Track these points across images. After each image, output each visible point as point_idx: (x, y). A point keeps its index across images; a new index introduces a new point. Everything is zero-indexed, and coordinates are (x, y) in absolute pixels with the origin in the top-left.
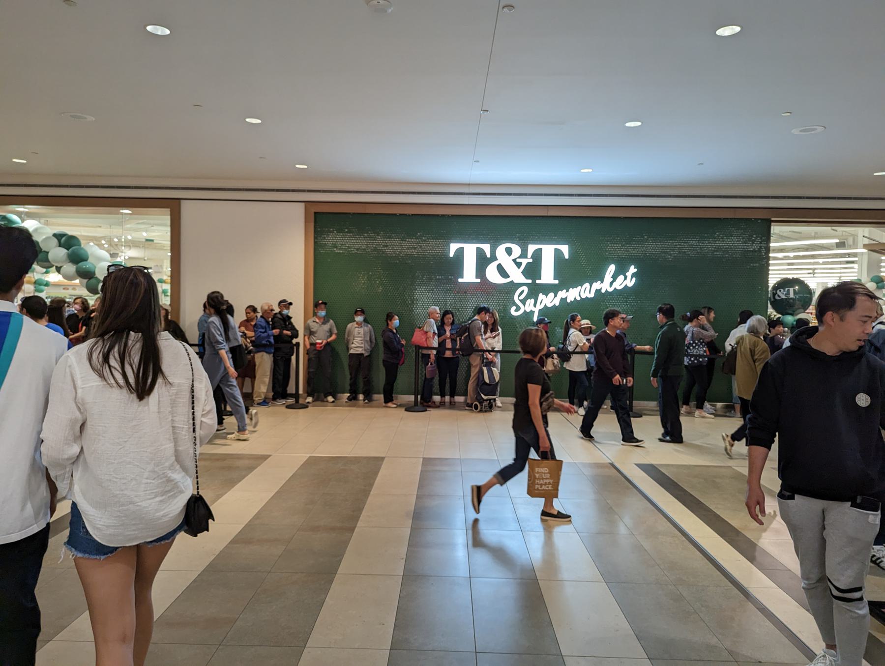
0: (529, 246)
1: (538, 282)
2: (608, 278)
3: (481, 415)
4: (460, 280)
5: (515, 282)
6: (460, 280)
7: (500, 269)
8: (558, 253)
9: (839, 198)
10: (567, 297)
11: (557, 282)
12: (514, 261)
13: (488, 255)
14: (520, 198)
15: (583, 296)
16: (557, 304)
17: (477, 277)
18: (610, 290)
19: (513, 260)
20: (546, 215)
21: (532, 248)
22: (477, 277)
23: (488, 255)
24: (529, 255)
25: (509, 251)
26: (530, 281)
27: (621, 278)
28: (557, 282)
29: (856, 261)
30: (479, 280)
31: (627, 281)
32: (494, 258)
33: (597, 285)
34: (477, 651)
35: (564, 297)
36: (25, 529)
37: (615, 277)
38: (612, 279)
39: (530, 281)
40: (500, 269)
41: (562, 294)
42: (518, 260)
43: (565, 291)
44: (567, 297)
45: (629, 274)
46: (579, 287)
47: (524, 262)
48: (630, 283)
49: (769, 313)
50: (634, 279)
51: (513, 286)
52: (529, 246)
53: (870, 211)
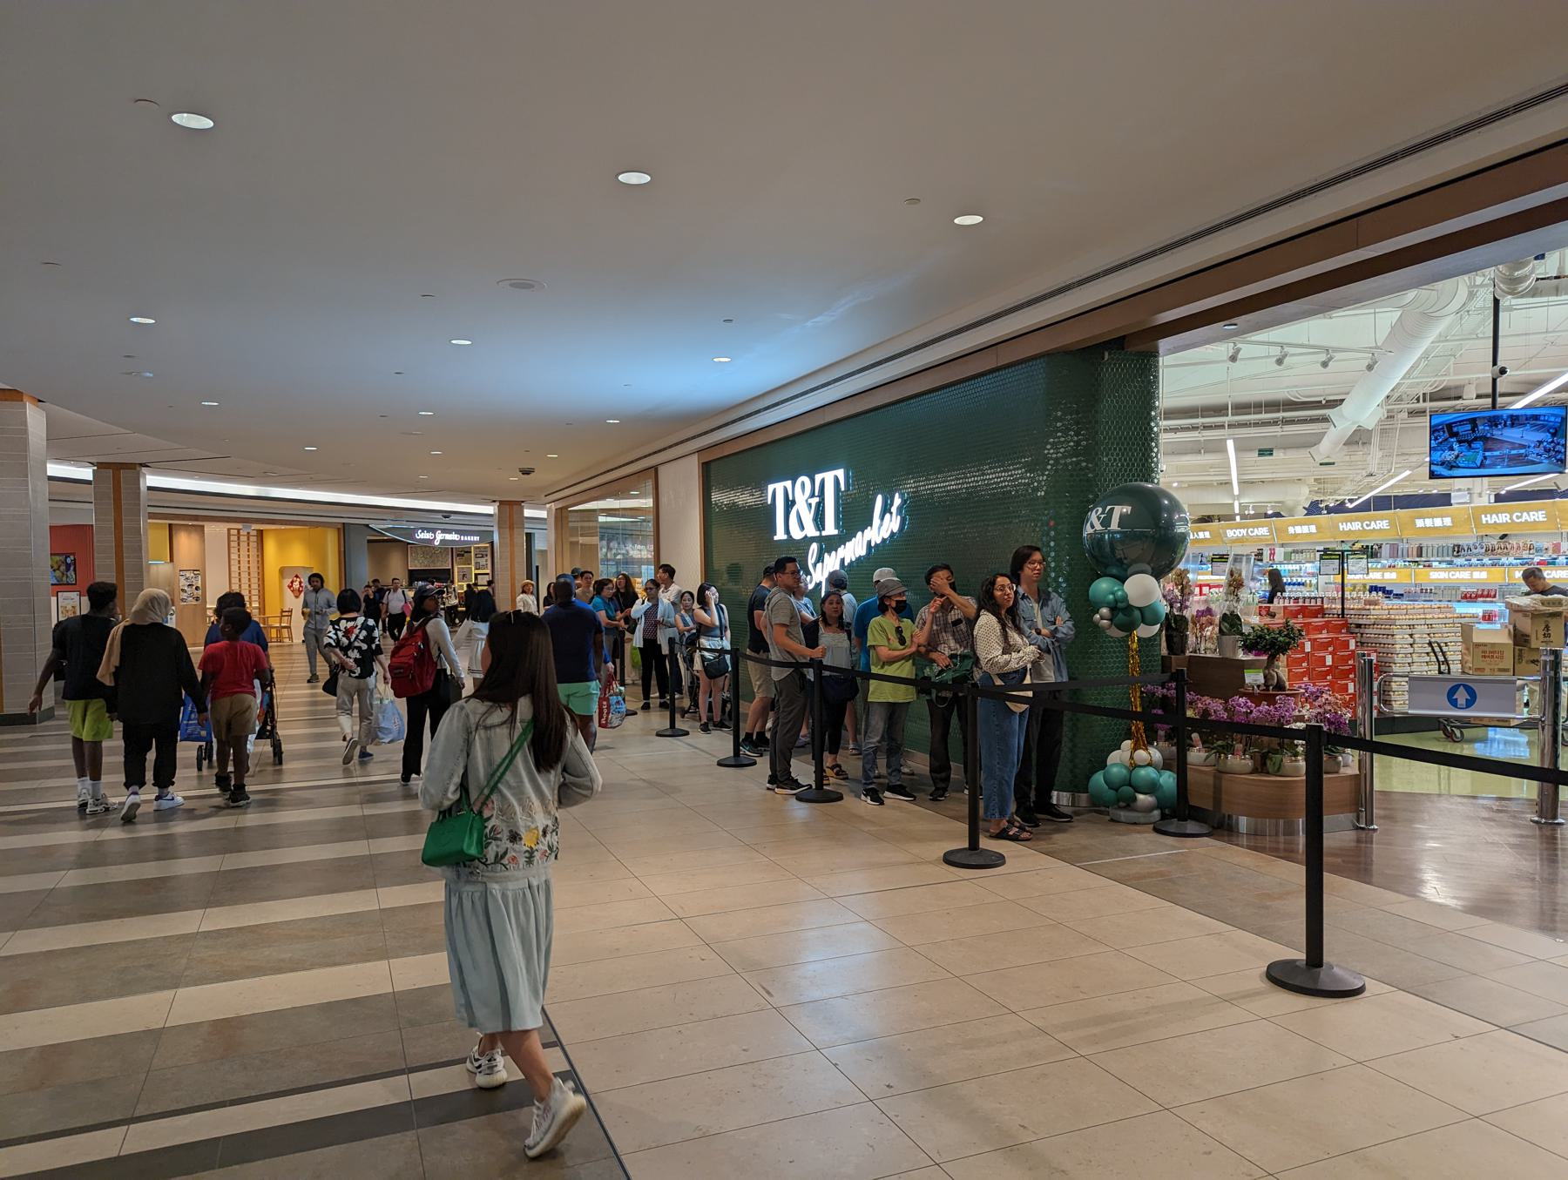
21: (818, 477)
31: (892, 524)
37: (882, 518)
45: (894, 509)
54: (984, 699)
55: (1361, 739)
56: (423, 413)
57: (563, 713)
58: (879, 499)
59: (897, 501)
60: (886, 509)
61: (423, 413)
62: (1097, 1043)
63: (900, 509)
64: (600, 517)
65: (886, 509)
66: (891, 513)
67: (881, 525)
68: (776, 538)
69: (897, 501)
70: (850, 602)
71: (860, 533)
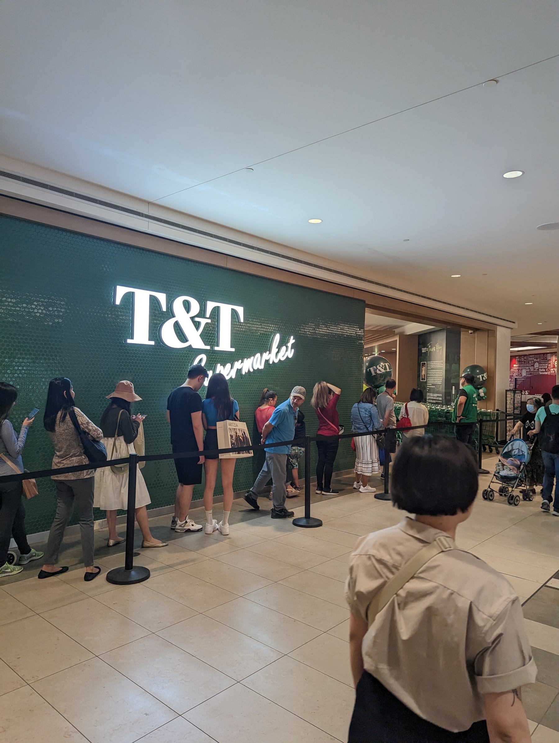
0: (243, 308)
1: (216, 348)
2: (274, 349)
3: (224, 490)
4: (129, 341)
5: (194, 347)
6: (129, 341)
7: (178, 328)
8: (234, 313)
9: (392, 288)
10: (242, 368)
11: (233, 350)
12: (192, 318)
13: (164, 309)
14: (322, 271)
15: (256, 368)
16: (234, 377)
17: (150, 339)
18: (276, 361)
19: (191, 318)
20: (352, 296)
21: (211, 305)
22: (150, 339)
23: (164, 309)
24: (208, 315)
25: (187, 306)
26: (208, 348)
27: (284, 348)
28: (233, 350)
29: (555, 344)
30: (152, 343)
31: (288, 353)
32: (170, 314)
33: (266, 356)
34: (484, 423)
35: (239, 368)
36: (265, 493)
37: (279, 347)
38: (277, 350)
39: (208, 348)
40: (178, 328)
41: (238, 365)
42: (197, 319)
43: (240, 361)
44: (242, 368)
45: (289, 345)
46: (253, 357)
47: (203, 322)
48: (290, 354)
49: (84, 450)
50: (293, 350)
51: (192, 352)
52: (243, 308)
53: (397, 300)
54: (311, 475)
55: (36, 496)
56: (457, 276)
57: (459, 405)
58: (277, 337)
59: (292, 341)
60: (283, 343)
61: (457, 276)
62: (418, 385)
63: (293, 346)
64: (154, 344)
65: (283, 343)
66: (287, 347)
67: (278, 352)
68: (219, 365)
69: (292, 341)
70: (101, 525)
71: (258, 355)
